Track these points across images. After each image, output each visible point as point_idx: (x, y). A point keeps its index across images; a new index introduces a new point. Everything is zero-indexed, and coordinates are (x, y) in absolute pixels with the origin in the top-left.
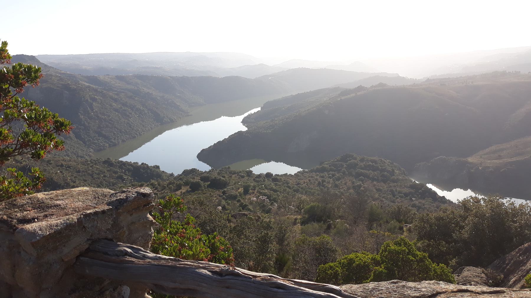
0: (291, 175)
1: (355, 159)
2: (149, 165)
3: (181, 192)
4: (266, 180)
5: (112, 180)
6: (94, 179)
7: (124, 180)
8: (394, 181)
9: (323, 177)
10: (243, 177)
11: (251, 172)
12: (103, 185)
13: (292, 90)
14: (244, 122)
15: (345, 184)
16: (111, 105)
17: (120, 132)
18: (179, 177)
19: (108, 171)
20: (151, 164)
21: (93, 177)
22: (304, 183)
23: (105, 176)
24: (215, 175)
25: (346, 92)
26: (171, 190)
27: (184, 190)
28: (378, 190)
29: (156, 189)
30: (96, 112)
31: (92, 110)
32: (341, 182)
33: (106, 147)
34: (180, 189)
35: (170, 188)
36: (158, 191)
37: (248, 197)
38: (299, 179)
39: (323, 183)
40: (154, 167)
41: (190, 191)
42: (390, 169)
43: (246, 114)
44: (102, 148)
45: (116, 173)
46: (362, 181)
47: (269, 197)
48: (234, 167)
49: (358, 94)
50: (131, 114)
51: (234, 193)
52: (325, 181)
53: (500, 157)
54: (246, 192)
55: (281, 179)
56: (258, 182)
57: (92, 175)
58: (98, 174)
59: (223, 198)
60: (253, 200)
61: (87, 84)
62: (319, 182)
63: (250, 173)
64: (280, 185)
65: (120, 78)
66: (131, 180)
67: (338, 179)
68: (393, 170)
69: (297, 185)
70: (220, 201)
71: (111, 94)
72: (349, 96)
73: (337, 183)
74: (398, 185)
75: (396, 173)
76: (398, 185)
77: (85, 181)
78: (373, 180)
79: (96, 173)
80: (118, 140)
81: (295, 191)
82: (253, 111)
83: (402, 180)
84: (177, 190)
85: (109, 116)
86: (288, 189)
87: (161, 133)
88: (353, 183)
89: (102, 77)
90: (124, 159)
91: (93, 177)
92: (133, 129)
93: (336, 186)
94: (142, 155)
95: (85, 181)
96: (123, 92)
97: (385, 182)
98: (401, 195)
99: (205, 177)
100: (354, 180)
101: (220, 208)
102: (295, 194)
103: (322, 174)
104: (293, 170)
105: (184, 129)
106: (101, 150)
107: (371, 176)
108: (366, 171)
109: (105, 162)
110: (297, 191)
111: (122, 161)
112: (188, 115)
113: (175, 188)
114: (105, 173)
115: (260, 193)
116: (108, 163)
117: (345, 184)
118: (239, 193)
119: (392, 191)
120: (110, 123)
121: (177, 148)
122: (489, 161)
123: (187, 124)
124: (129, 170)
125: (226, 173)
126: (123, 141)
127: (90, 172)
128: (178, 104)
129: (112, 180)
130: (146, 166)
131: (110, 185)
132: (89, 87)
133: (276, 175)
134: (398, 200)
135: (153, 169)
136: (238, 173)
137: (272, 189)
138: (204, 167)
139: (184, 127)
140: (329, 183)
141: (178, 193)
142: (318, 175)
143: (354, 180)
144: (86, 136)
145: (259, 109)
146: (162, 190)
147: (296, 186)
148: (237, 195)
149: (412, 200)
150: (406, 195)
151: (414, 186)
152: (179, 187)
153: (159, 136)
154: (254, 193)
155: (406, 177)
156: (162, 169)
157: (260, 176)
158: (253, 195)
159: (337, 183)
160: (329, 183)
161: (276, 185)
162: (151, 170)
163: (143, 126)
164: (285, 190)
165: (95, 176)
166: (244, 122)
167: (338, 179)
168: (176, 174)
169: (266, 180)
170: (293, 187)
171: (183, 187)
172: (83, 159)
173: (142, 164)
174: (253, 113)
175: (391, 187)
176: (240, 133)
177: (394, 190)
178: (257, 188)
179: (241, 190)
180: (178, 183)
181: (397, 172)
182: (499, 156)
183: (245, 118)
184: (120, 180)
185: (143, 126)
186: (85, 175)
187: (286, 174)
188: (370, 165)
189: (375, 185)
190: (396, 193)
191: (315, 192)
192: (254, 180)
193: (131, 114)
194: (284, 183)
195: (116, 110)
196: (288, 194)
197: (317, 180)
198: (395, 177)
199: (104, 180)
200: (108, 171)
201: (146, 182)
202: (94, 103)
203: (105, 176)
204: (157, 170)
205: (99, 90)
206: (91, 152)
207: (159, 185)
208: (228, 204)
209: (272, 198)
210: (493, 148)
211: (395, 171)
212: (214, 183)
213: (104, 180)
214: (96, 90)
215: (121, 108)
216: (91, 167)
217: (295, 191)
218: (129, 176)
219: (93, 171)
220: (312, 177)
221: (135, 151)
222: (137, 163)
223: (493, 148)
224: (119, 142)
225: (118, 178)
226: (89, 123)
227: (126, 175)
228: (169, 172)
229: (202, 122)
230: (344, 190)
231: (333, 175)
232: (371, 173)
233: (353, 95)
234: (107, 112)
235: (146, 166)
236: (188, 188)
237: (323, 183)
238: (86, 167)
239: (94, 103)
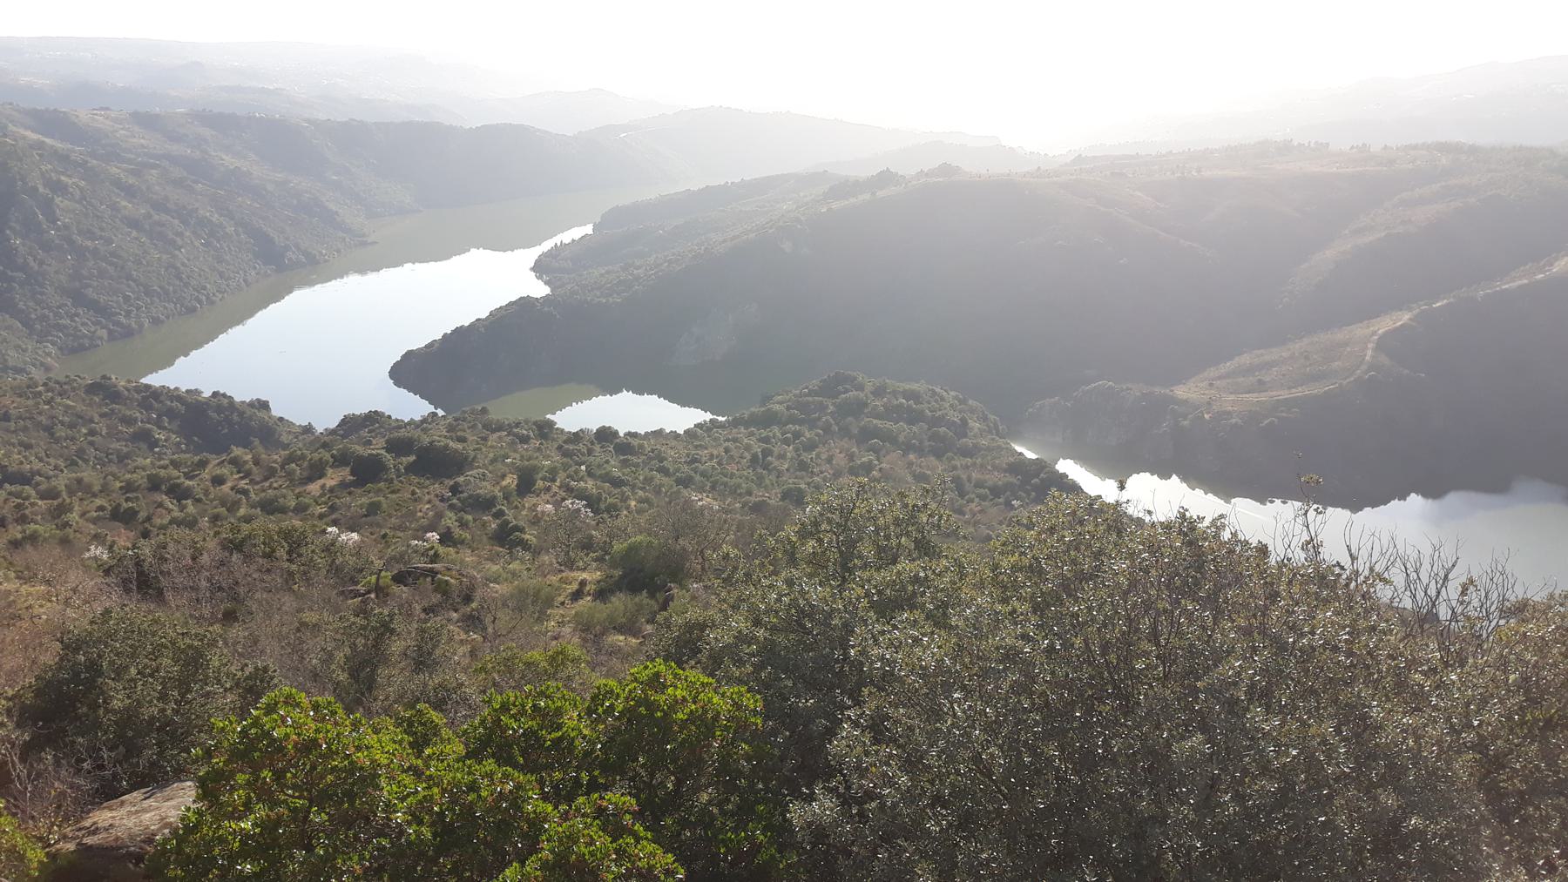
0: (675, 435)
1: (861, 388)
2: (237, 399)
4: (597, 448)
5: (115, 445)
6: (57, 441)
7: (155, 443)
8: (966, 452)
9: (766, 440)
10: (525, 440)
11: (551, 424)
12: (86, 461)
13: (690, 174)
14: (540, 268)
16: (114, 207)
20: (241, 395)
21: (52, 435)
23: (92, 433)
25: (846, 187)
26: (292, 481)
27: (332, 478)
29: (248, 474)
30: (66, 227)
31: (53, 220)
32: (818, 456)
33: (101, 338)
35: (290, 474)
36: (252, 482)
37: (529, 501)
38: (696, 447)
39: (765, 457)
40: (251, 404)
41: (352, 484)
42: (955, 417)
43: (547, 246)
44: (87, 342)
45: (129, 421)
46: (876, 450)
47: (593, 503)
48: (508, 408)
49: (880, 194)
50: (180, 235)
51: (486, 489)
52: (770, 453)
53: (1261, 386)
54: (526, 484)
55: (641, 446)
56: (566, 454)
57: (49, 430)
58: (72, 426)
59: (452, 507)
60: (543, 512)
61: (34, 136)
62: (755, 457)
63: (545, 430)
64: (637, 465)
66: (179, 444)
68: (964, 422)
69: (689, 463)
70: (439, 516)
71: (114, 170)
72: (853, 200)
73: (806, 457)
74: (974, 464)
76: (974, 464)
77: (28, 447)
78: (907, 448)
80: (138, 316)
81: (679, 482)
82: (567, 237)
83: (989, 449)
85: (109, 241)
87: (277, 298)
90: (155, 380)
91: (52, 435)
92: (186, 285)
93: (803, 466)
94: (216, 367)
95: (28, 447)
97: (939, 455)
98: (982, 491)
99: (401, 439)
102: (679, 492)
104: (680, 418)
105: (352, 283)
106: (82, 348)
107: (901, 438)
108: (889, 425)
109: (93, 389)
110: (685, 482)
111: (148, 387)
112: (364, 244)
113: (305, 474)
114: (91, 421)
115: (569, 490)
116: (103, 390)
117: (829, 460)
118: (503, 489)
120: (111, 264)
121: (319, 351)
122: (1232, 397)
123: (362, 271)
124: (171, 414)
125: (473, 427)
126: (156, 321)
128: (332, 206)
129: (115, 445)
132: (40, 145)
133: (629, 434)
134: (973, 505)
135: (249, 412)
136: (509, 428)
137: (607, 478)
138: (410, 407)
139: (353, 280)
140: (782, 457)
141: (314, 488)
142: (752, 434)
144: (31, 304)
146: (266, 479)
147: (686, 468)
148: (495, 497)
149: (1013, 508)
150: (996, 492)
151: (1019, 467)
152: (317, 471)
154: (548, 489)
155: (1001, 442)
156: (276, 411)
157: (577, 437)
158: (547, 497)
159: (806, 457)
160: (782, 457)
161: (625, 463)
162: (241, 414)
164: (648, 480)
165: (61, 432)
166: (540, 268)
167: (810, 447)
168: (320, 429)
169: (597, 448)
170: (678, 470)
171: (330, 471)
172: (24, 377)
173: (215, 394)
174: (567, 240)
175: (955, 468)
176: (524, 304)
177: (964, 477)
179: (511, 481)
180: (316, 456)
181: (975, 425)
182: (1260, 382)
183: (544, 255)
184: (144, 446)
186: (25, 429)
189: (910, 464)
191: (739, 486)
192: (560, 448)
193: (180, 235)
194: (651, 459)
195: (134, 224)
197: (748, 448)
199: (92, 444)
201: (218, 453)
202: (58, 200)
203: (92, 433)
206: (49, 354)
208: (463, 525)
210: (1245, 359)
212: (428, 458)
213: (92, 444)
214: (64, 158)
215: (150, 216)
216: (48, 403)
217: (679, 482)
218: (171, 431)
220: (735, 440)
221: (194, 353)
222: (197, 392)
223: (1245, 359)
224: (141, 326)
226: (41, 263)
227: (164, 428)
228: (300, 420)
229: (408, 266)
230: (825, 480)
231: (797, 435)
232: (902, 429)
234: (102, 229)
236: (345, 473)
237: (765, 457)
238: (30, 402)
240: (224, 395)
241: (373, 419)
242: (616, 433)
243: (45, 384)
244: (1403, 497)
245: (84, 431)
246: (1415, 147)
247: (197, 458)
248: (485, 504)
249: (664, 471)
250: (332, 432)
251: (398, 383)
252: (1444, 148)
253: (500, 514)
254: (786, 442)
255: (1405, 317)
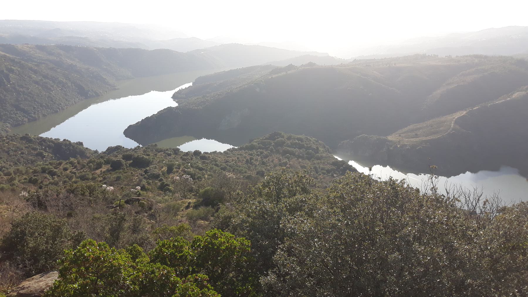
0: (220, 153)
1: (283, 137)
2: (72, 142)
3: (101, 171)
4: (194, 158)
5: (30, 158)
7: (44, 157)
8: (318, 158)
9: (251, 155)
10: (169, 155)
11: (178, 149)
12: (20, 163)
13: (224, 66)
14: (174, 97)
15: (272, 161)
17: (41, 106)
18: (102, 156)
19: (26, 147)
20: (73, 140)
21: (9, 154)
22: (233, 160)
23: (22, 153)
24: (140, 154)
27: (104, 168)
28: (303, 167)
29: (75, 167)
30: (13, 84)
31: (9, 81)
32: (269, 160)
33: (25, 121)
34: (101, 167)
35: (90, 167)
36: (77, 170)
37: (171, 175)
41: (111, 170)
42: (314, 147)
43: (177, 90)
44: (20, 123)
46: (288, 158)
47: (193, 176)
48: (163, 144)
49: (289, 72)
50: (53, 86)
51: (156, 171)
52: (253, 159)
53: (416, 136)
54: (170, 170)
55: (209, 157)
56: (183, 160)
57: (8, 152)
59: (145, 178)
61: (3, 53)
63: (177, 151)
64: (208, 163)
65: (41, 48)
66: (52, 157)
67: (266, 157)
68: (318, 148)
69: (225, 162)
71: (30, 65)
72: (280, 74)
73: (265, 160)
74: (321, 162)
75: (320, 151)
76: (321, 162)
78: (299, 157)
79: (12, 150)
80: (38, 114)
81: (222, 169)
82: (184, 87)
84: (97, 169)
86: (215, 167)
87: (85, 107)
88: (280, 160)
89: (19, 46)
90: (44, 135)
91: (9, 154)
93: (264, 163)
94: (65, 131)
96: (44, 63)
97: (309, 159)
99: (128, 155)
100: (281, 158)
101: (139, 188)
103: (250, 152)
104: (222, 147)
107: (297, 154)
109: (22, 138)
110: (224, 169)
111: (41, 138)
112: (116, 89)
113: (95, 167)
114: (22, 149)
115: (185, 172)
116: (26, 139)
117: (272, 161)
118: (162, 172)
119: (315, 168)
121: (101, 125)
123: (114, 98)
124: (50, 147)
125: (152, 151)
126: (44, 116)
127: (5, 148)
130: (68, 143)
131: (29, 163)
132: (5, 56)
133: (205, 153)
134: (320, 176)
136: (164, 151)
138: (130, 144)
139: (111, 102)
140: (256, 160)
141: (98, 172)
142: (246, 153)
143: (281, 158)
145: (191, 84)
146: (82, 169)
147: (224, 164)
149: (334, 177)
150: (328, 171)
151: (336, 163)
152: (99, 166)
153: (80, 113)
154: (178, 172)
156: (85, 146)
157: (187, 154)
158: (177, 174)
160: (256, 160)
161: (204, 163)
162: (73, 147)
163: (66, 100)
164: (211, 168)
165: (12, 153)
166: (174, 97)
167: (266, 157)
169: (194, 158)
170: (221, 165)
171: (103, 166)
173: (64, 140)
174: (184, 88)
175: (315, 164)
177: (318, 167)
178: (182, 167)
179: (165, 169)
180: (99, 161)
181: (321, 149)
185: (66, 100)
187: (216, 151)
188: (296, 143)
189: (300, 162)
190: (319, 170)
191: (242, 170)
193: (53, 86)
194: (212, 161)
195: (37, 83)
196: (215, 172)
198: (319, 155)
199: (22, 157)
200: (26, 147)
202: (11, 75)
203: (22, 153)
204: (80, 147)
205: (16, 60)
206: (7, 127)
207: (78, 163)
208: (149, 184)
209: (196, 177)
210: (411, 127)
211: (320, 149)
212: (135, 161)
213: (22, 157)
214: (13, 61)
215: (42, 80)
217: (222, 169)
219: (9, 148)
220: (241, 155)
221: (57, 126)
222: (58, 139)
223: (411, 127)
224: (39, 117)
225: (37, 155)
227: (47, 152)
228: (93, 149)
229: (130, 97)
230: (271, 168)
231: (262, 153)
232: (297, 151)
233: (284, 73)
235: (68, 143)
236: (109, 167)
239: (11, 75)
240: (67, 140)
241: (118, 148)
242: (200, 153)
243: (6, 137)
244: (464, 173)
245: (20, 153)
246: (467, 56)
247: (58, 162)
248: (156, 177)
249: (217, 165)
250: (104, 153)
251: (126, 136)
252: (476, 56)
253: (161, 180)
254: (258, 155)
255: (464, 113)
